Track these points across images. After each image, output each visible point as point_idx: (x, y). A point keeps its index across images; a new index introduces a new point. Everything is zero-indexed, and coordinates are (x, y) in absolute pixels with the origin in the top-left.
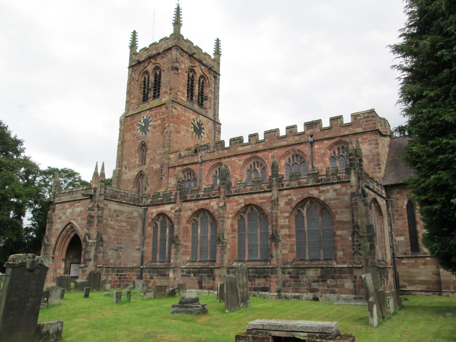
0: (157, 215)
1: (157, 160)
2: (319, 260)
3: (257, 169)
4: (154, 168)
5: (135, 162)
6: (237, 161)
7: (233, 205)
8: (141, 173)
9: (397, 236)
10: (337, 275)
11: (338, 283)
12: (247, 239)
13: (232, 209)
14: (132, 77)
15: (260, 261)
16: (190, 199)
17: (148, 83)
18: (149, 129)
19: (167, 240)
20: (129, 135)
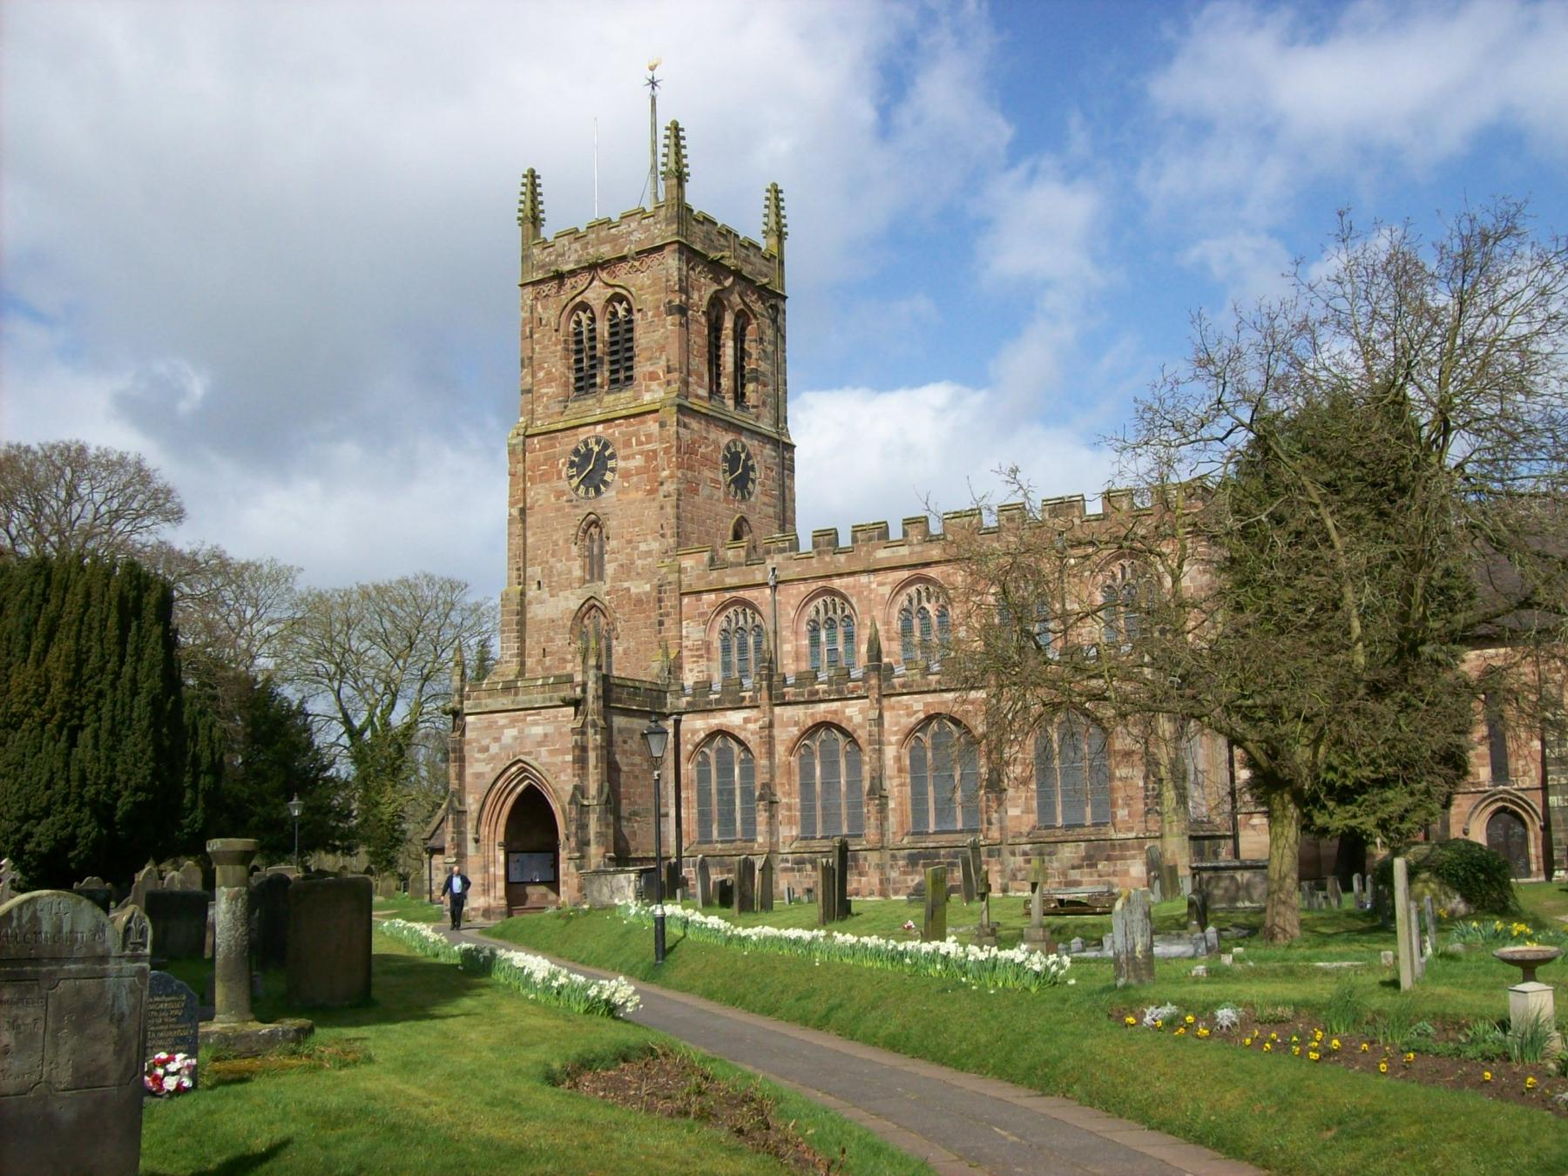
0: (707, 736)
1: (640, 571)
2: (1082, 826)
3: (927, 606)
4: (633, 590)
5: (570, 572)
6: (874, 586)
7: (900, 715)
8: (592, 602)
10: (1117, 853)
11: (1118, 868)
12: (931, 789)
13: (897, 724)
14: (535, 315)
15: (961, 831)
17: (593, 339)
18: (606, 478)
19: (738, 792)
20: (542, 491)
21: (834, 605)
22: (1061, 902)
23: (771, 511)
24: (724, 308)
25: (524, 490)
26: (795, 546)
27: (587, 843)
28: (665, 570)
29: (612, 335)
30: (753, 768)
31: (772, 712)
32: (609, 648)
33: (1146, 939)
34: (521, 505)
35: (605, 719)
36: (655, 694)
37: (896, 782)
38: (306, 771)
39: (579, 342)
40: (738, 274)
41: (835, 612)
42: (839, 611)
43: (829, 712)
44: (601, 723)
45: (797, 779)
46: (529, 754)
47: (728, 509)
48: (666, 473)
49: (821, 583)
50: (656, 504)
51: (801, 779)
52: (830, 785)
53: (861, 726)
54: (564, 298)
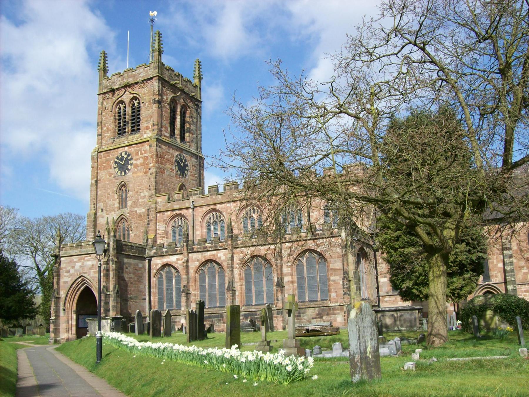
0: (162, 266)
2: (317, 301)
3: (254, 215)
4: (138, 211)
5: (114, 205)
8: (122, 216)
9: (381, 277)
12: (253, 287)
14: (103, 106)
16: (197, 250)
17: (125, 115)
19: (174, 289)
21: (217, 216)
22: (308, 330)
23: (194, 182)
24: (177, 104)
25: (97, 173)
26: (202, 192)
27: (109, 310)
28: (150, 203)
29: (132, 113)
30: (180, 279)
31: (188, 256)
32: (128, 235)
33: (374, 342)
34: (96, 179)
35: (117, 258)
36: (140, 249)
37: (239, 284)
38: (15, 287)
39: (120, 116)
40: (182, 91)
41: (217, 218)
42: (219, 218)
43: (211, 255)
44: (115, 259)
45: (198, 283)
46: (86, 273)
47: (177, 181)
48: (151, 165)
49: (211, 207)
50: (147, 177)
51: (200, 283)
52: (212, 286)
53: (225, 261)
54: (115, 99)
